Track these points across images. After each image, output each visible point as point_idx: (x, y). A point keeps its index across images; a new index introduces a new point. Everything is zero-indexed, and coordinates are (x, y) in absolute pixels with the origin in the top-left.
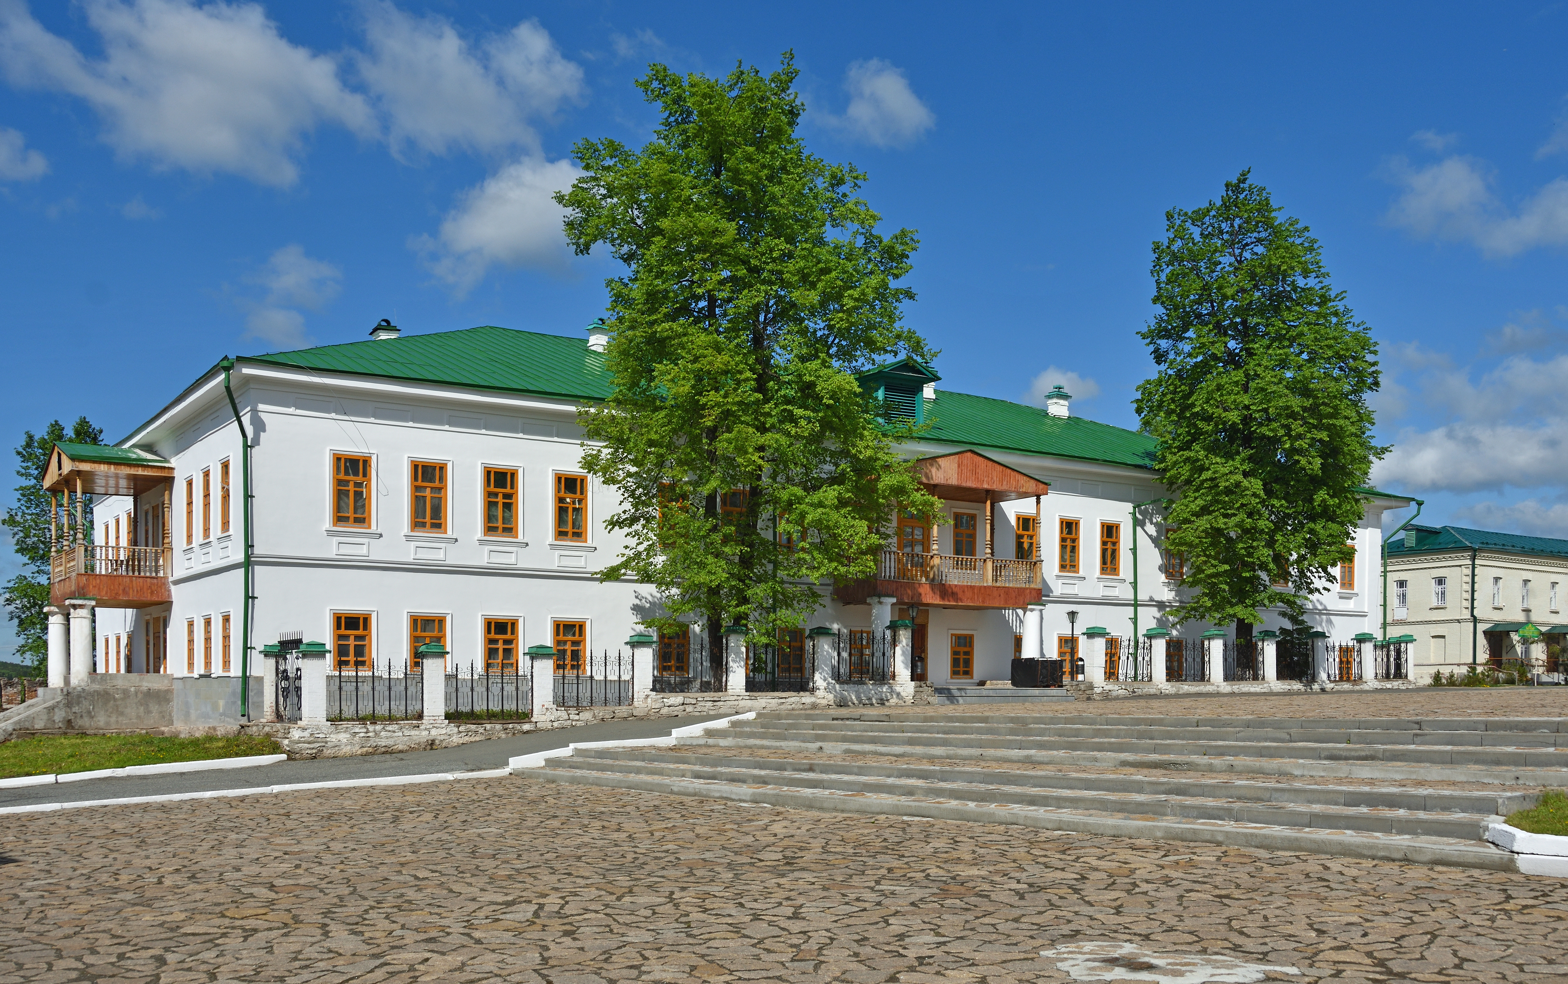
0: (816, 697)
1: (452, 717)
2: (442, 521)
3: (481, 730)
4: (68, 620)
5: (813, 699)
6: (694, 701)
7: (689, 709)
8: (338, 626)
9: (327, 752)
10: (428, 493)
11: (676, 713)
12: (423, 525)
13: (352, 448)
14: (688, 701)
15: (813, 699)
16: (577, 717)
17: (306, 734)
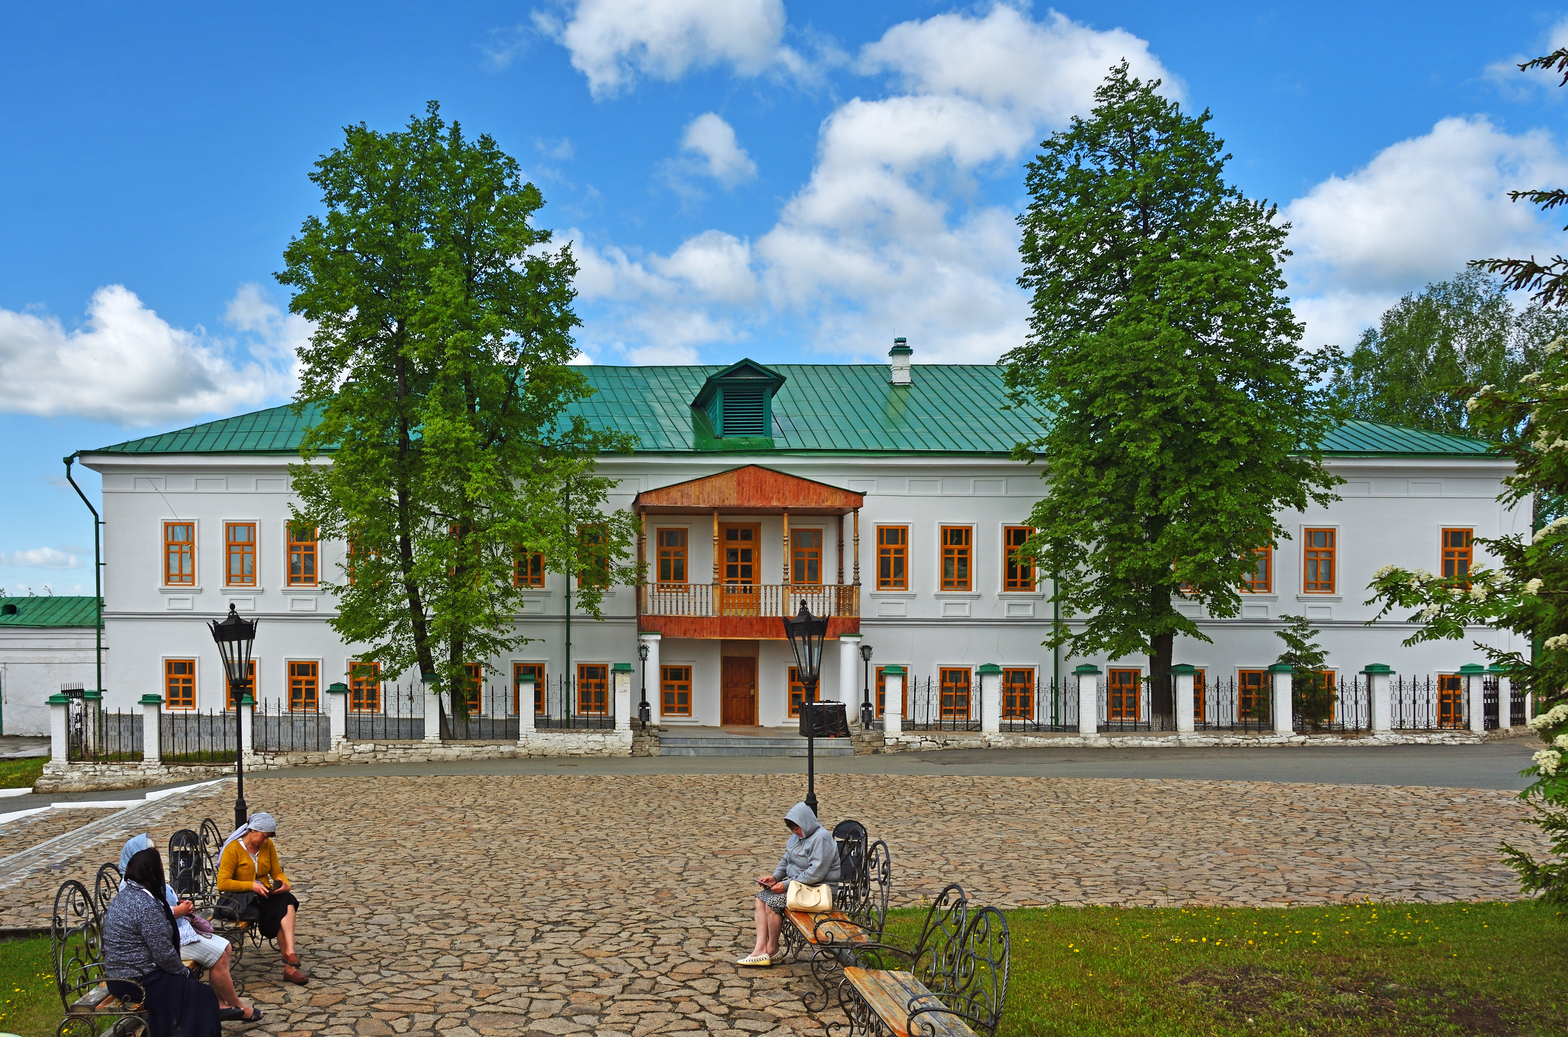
0: (515, 745)
2: (967, 579)
3: (187, 772)
5: (512, 748)
6: (384, 748)
7: (380, 756)
11: (366, 760)
12: (1015, 584)
14: (378, 748)
15: (512, 748)
16: (271, 762)
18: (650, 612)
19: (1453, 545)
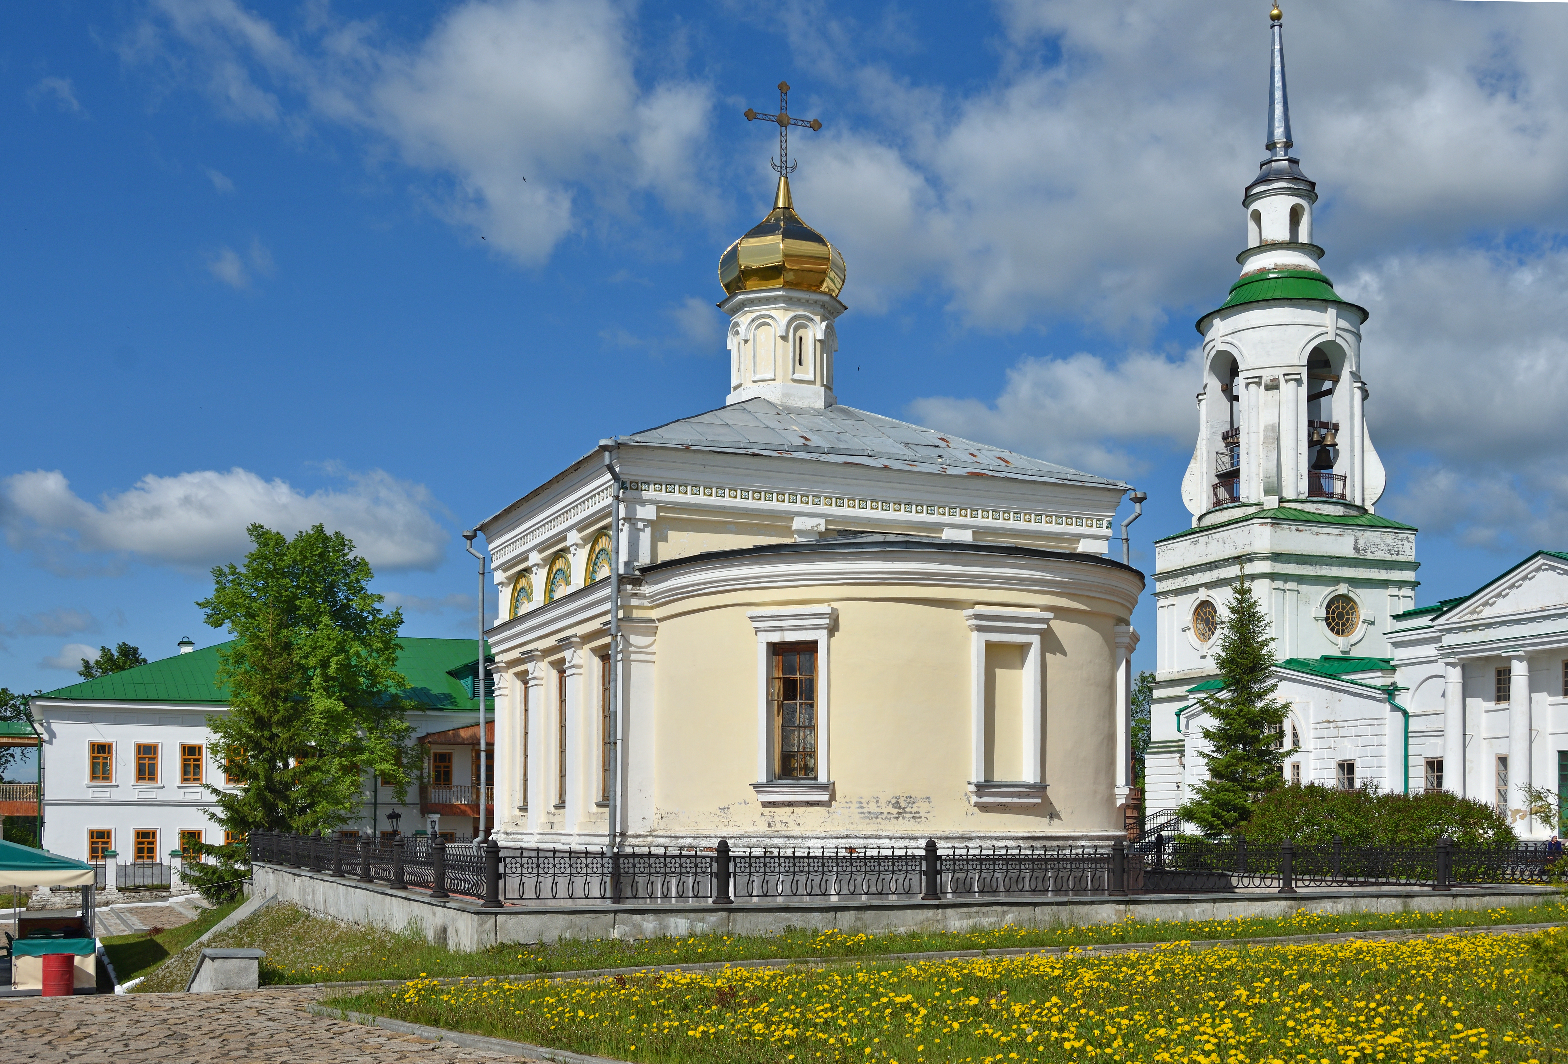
1: (120, 890)
4: (526, 689)
8: (92, 837)
9: (48, 907)
10: (147, 761)
12: (144, 779)
13: (100, 739)
17: (38, 897)
18: (433, 801)
19: (99, 752)
